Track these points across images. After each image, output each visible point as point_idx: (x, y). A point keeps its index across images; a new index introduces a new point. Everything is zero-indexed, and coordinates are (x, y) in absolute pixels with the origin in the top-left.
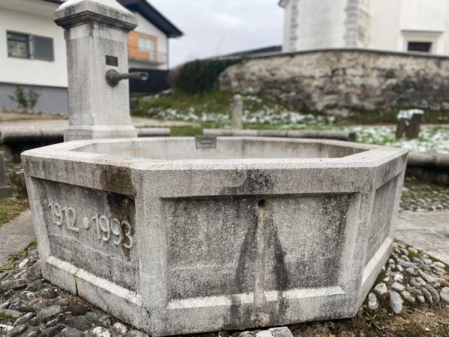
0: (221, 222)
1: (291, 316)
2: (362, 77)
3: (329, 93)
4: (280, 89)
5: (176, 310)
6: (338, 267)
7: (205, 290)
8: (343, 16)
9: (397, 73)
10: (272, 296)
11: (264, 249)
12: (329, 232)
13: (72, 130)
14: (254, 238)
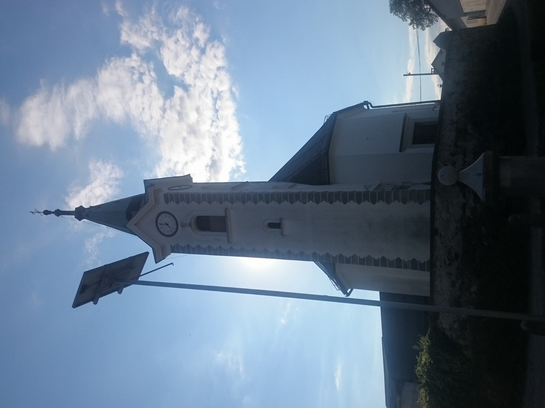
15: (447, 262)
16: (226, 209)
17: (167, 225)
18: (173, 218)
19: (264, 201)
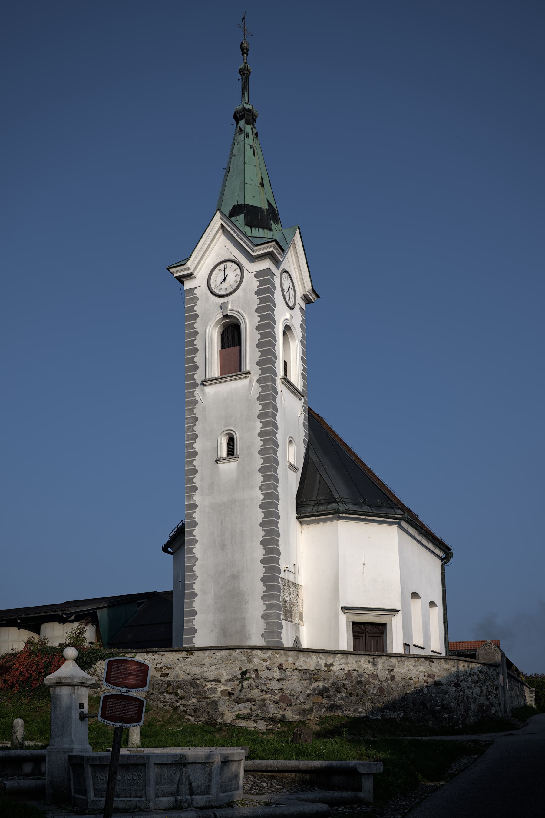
0: (171, 772)
1: (195, 804)
2: (279, 680)
3: (239, 701)
4: (176, 694)
5: (158, 800)
6: (210, 788)
7: (166, 795)
8: (260, 588)
9: (322, 675)
10: (189, 797)
11: (185, 781)
12: (206, 775)
13: (55, 749)
14: (182, 777)
15: (159, 666)
16: (249, 373)
17: (224, 280)
18: (234, 287)
19: (261, 394)
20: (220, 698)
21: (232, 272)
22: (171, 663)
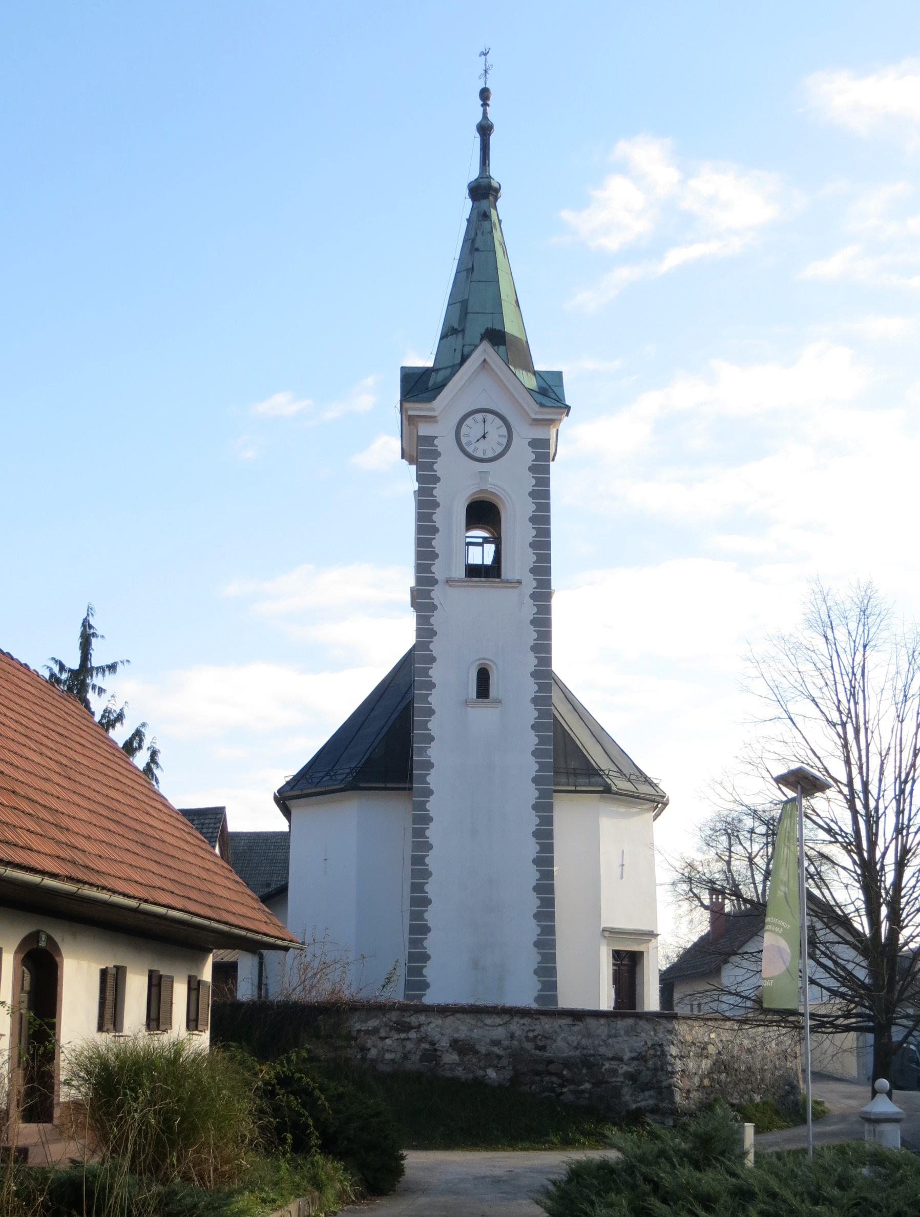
15: (531, 1035)
20: (622, 1082)
21: (495, 429)
22: (550, 1032)
